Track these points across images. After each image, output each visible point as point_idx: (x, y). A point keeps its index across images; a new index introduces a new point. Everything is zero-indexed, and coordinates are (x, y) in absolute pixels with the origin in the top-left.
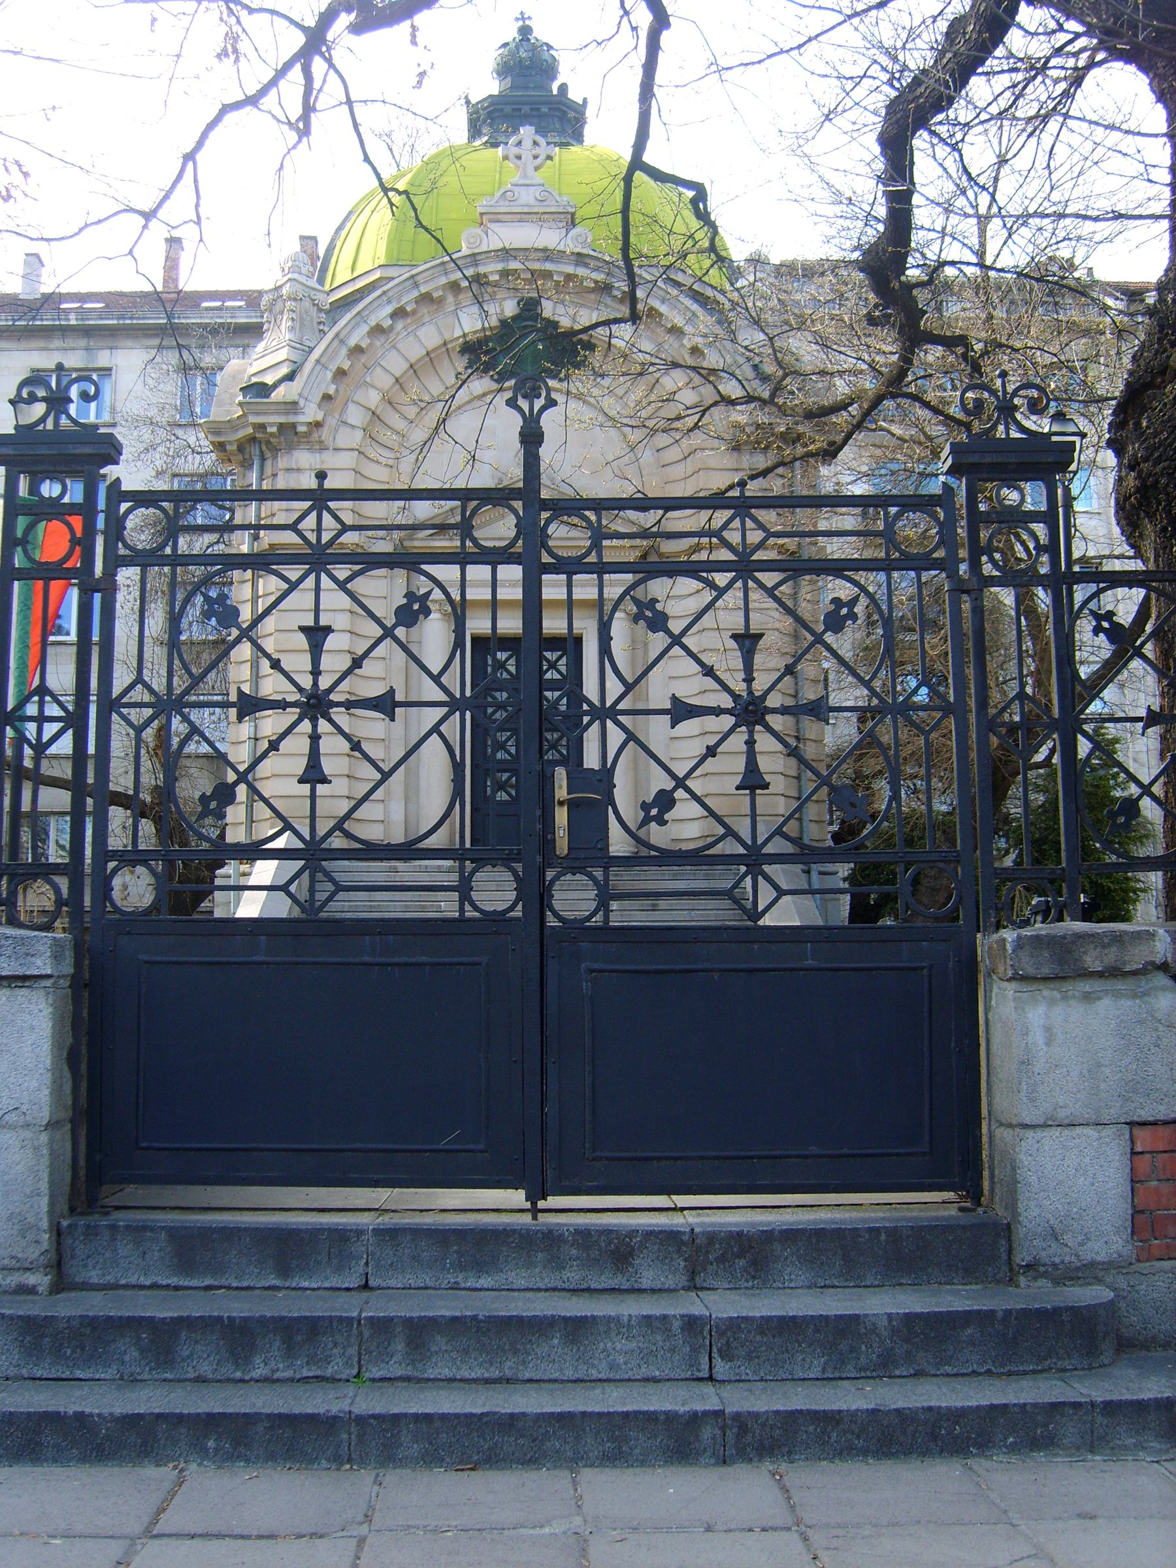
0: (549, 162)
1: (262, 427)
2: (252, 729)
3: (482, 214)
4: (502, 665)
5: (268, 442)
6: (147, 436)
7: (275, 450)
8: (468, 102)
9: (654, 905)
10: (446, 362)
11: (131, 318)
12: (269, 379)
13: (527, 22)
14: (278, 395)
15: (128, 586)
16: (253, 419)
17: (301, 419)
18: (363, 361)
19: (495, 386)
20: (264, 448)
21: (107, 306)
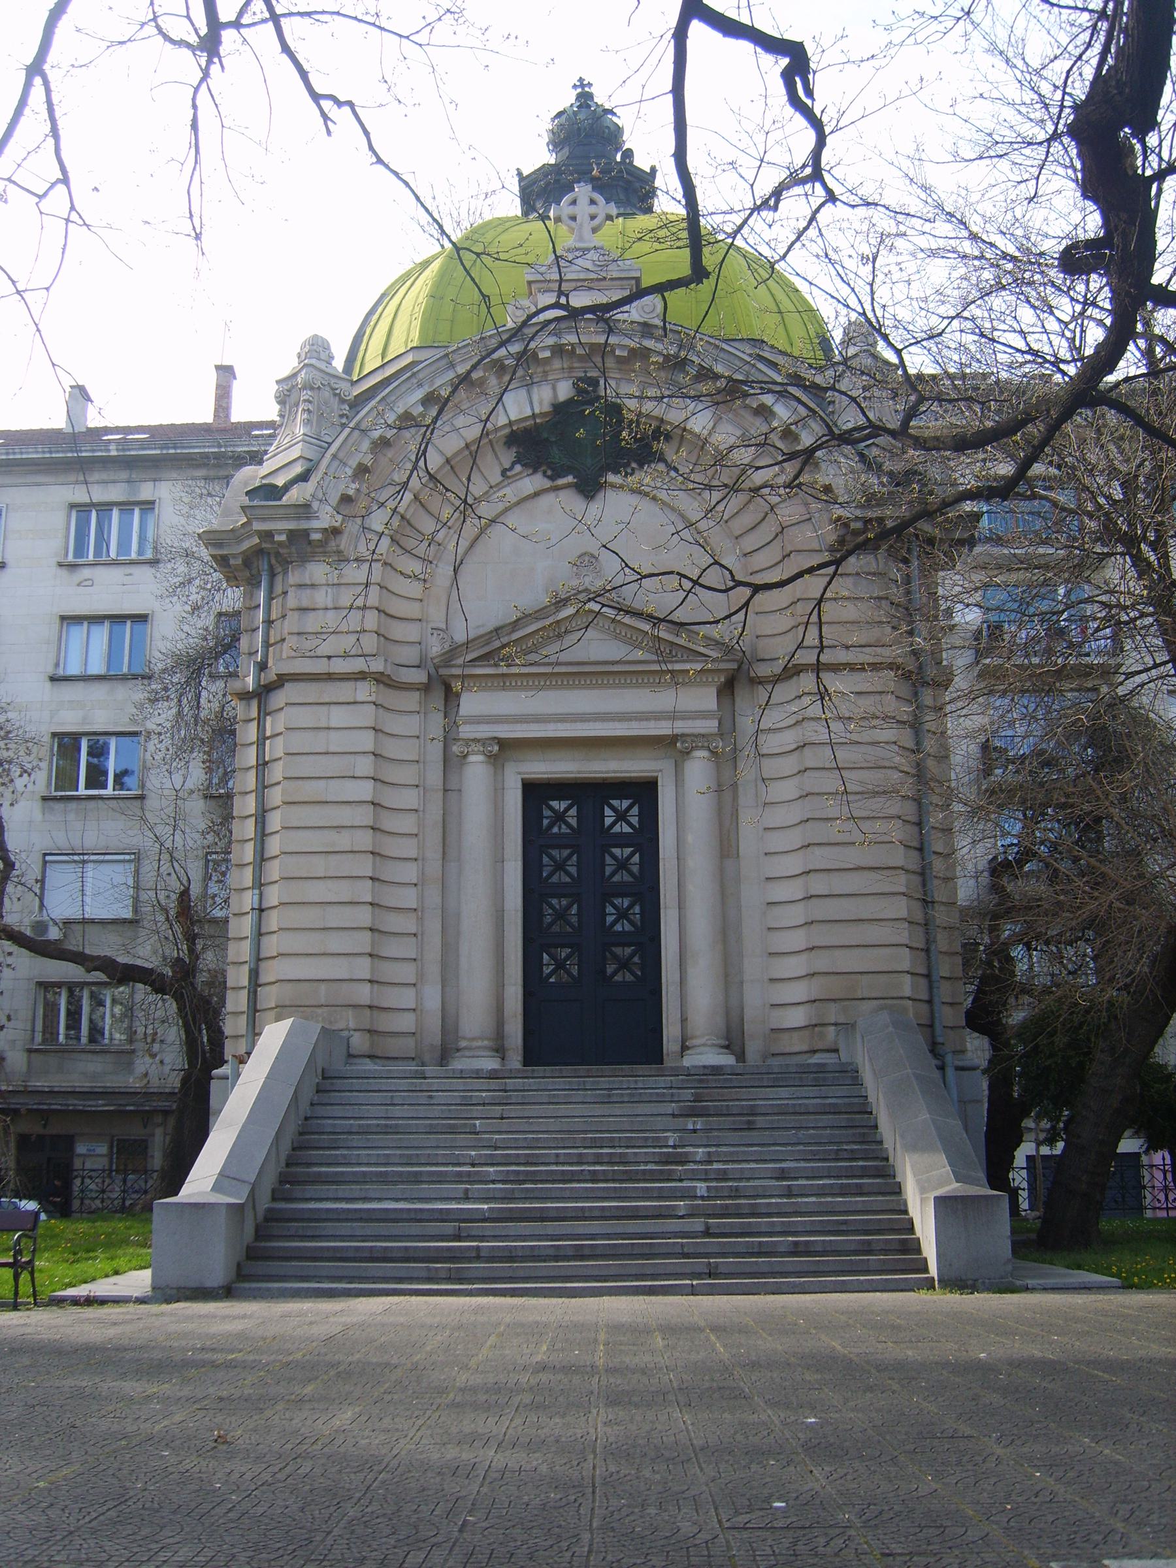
0: (608, 222)
1: (268, 535)
2: (256, 898)
3: (530, 283)
4: (560, 817)
5: (278, 554)
6: (182, 569)
7: (286, 563)
8: (519, 174)
9: (749, 1122)
10: (490, 456)
11: (175, 448)
12: (280, 481)
13: (587, 89)
14: (294, 495)
15: (160, 734)
16: (257, 526)
17: (316, 524)
18: (390, 455)
19: (548, 484)
20: (273, 561)
21: (152, 436)
